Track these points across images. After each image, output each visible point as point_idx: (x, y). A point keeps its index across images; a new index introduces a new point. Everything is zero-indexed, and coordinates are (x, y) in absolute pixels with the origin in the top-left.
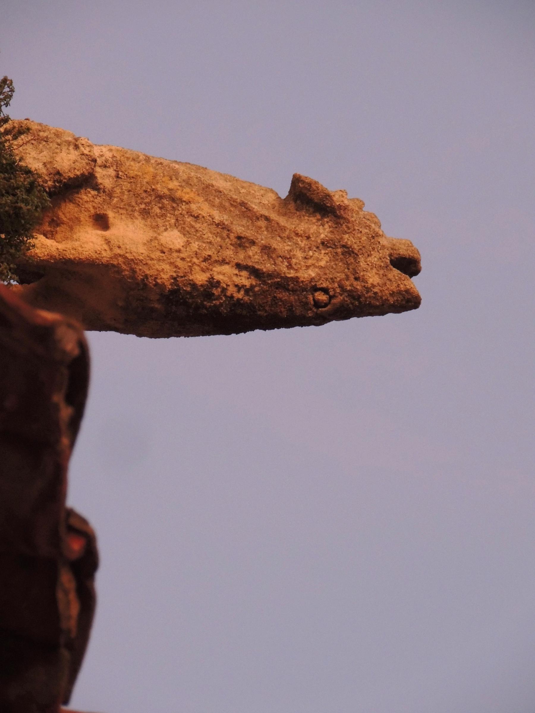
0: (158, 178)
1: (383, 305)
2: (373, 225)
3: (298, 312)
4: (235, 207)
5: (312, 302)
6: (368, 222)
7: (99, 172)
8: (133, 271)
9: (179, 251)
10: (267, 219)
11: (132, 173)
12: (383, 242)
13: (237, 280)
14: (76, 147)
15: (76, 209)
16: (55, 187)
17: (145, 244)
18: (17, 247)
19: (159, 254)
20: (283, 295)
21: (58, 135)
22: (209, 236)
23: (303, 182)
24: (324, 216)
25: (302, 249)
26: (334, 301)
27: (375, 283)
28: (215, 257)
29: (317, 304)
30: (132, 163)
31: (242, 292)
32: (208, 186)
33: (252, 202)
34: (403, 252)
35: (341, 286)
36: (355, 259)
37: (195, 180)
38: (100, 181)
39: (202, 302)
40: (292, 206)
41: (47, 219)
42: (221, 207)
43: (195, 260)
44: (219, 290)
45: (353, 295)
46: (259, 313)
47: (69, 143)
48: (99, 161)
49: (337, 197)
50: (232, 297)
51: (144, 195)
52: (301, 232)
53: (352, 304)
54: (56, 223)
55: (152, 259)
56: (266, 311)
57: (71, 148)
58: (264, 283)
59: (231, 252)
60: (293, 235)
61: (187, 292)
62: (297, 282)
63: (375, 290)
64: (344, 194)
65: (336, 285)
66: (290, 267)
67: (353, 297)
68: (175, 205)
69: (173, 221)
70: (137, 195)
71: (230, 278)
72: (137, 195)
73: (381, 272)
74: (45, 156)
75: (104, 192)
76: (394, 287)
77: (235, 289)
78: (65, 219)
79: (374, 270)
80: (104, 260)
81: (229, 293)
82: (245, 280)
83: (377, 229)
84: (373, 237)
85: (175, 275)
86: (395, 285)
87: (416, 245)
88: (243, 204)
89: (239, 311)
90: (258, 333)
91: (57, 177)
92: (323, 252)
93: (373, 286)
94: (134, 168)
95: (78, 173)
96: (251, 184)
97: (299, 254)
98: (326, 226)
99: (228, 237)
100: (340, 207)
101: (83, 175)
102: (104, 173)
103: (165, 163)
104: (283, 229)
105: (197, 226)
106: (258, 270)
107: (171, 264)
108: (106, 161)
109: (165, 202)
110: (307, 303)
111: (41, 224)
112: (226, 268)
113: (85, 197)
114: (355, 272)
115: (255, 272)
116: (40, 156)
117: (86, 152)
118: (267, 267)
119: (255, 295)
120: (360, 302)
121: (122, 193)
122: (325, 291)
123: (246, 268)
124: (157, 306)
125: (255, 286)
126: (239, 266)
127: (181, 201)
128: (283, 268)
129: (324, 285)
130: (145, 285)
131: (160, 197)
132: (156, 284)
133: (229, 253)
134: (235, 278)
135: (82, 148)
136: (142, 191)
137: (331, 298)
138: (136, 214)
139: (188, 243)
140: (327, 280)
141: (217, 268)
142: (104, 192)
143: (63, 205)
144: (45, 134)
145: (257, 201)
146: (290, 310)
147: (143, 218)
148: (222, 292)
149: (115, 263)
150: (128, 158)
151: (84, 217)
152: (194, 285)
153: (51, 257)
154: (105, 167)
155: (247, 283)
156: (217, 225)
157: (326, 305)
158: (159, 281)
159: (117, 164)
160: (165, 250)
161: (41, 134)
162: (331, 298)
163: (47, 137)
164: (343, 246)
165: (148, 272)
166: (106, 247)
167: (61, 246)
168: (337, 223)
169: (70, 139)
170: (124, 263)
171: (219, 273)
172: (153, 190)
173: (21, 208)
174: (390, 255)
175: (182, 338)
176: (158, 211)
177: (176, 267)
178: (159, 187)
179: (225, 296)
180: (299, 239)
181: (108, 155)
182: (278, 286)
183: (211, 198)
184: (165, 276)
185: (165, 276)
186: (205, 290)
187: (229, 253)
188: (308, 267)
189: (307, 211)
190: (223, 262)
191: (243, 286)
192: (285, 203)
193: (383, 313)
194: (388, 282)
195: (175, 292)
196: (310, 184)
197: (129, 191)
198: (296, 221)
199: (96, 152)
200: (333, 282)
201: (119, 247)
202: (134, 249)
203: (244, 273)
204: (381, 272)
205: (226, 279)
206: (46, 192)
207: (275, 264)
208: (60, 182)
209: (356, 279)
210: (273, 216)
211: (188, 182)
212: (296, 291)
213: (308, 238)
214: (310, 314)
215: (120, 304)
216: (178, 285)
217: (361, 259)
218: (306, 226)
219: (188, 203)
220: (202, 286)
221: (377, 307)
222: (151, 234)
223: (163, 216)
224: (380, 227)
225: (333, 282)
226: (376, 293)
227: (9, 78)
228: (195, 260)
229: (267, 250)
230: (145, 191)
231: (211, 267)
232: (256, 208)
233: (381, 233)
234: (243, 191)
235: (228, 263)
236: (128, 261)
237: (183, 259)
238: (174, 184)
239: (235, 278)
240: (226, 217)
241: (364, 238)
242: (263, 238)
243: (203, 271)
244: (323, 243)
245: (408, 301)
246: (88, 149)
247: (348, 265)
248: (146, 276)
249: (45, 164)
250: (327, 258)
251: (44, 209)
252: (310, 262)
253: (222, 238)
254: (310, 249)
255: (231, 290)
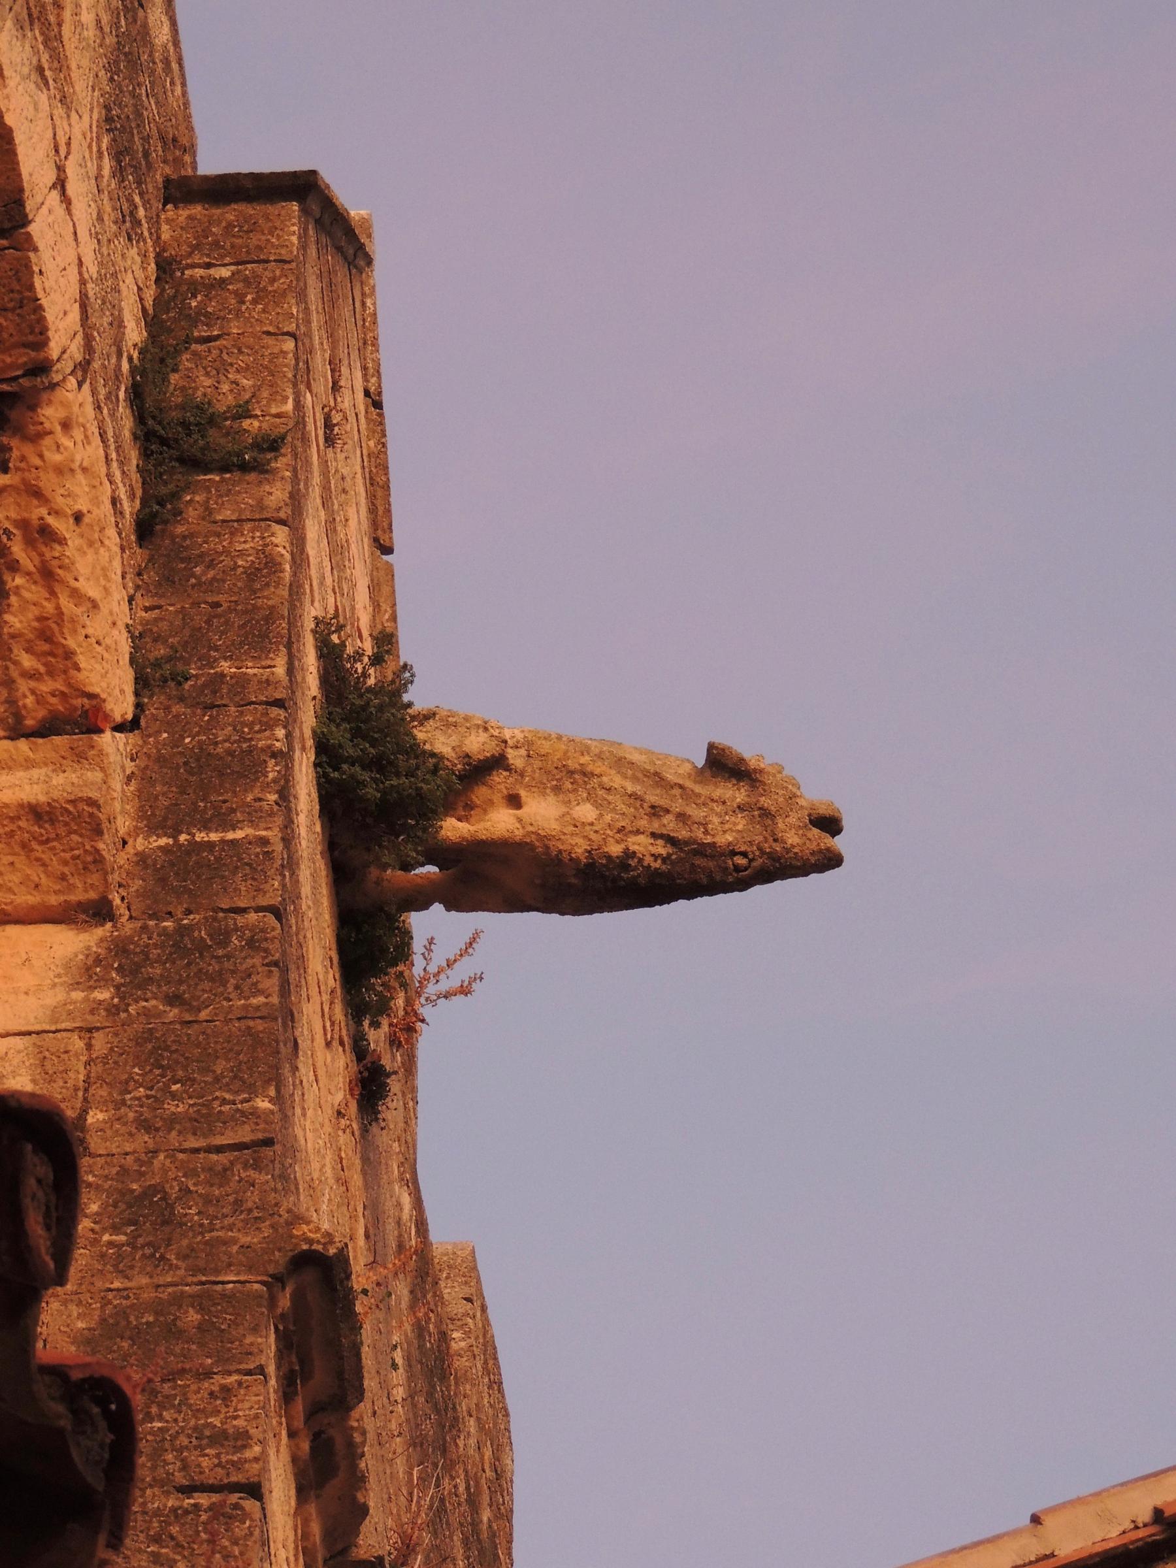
0: (570, 754)
1: (804, 865)
2: (790, 787)
3: (718, 878)
4: (648, 777)
5: (732, 866)
6: (785, 784)
7: (511, 754)
8: (547, 848)
9: (592, 824)
10: (681, 787)
11: (543, 752)
12: (802, 802)
13: (653, 850)
14: (486, 729)
15: (489, 792)
16: (465, 770)
17: (557, 820)
18: (425, 830)
19: (572, 828)
20: (699, 861)
21: (467, 719)
22: (622, 807)
23: (717, 748)
24: (739, 780)
25: (719, 815)
26: (754, 864)
27: (795, 844)
28: (629, 828)
29: (737, 869)
30: (544, 742)
31: (659, 861)
32: (620, 759)
33: (667, 772)
34: (823, 811)
35: (759, 849)
36: (772, 820)
37: (608, 754)
38: (511, 761)
39: (619, 874)
40: (708, 773)
41: (462, 804)
42: (635, 779)
43: (608, 832)
44: (636, 860)
45: (773, 857)
46: (678, 881)
47: (478, 726)
48: (510, 742)
49: (753, 761)
50: (649, 866)
51: (555, 771)
52: (716, 798)
53: (772, 865)
54: (470, 807)
55: (565, 834)
56: (685, 879)
57: (480, 731)
58: (681, 850)
59: (646, 822)
60: (708, 801)
61: (604, 865)
62: (715, 847)
63: (796, 850)
64: (761, 759)
65: (755, 848)
66: (706, 832)
67: (774, 860)
68: (586, 779)
69: (585, 795)
70: (548, 772)
71: (645, 847)
72: (548, 772)
73: (801, 832)
74: (454, 740)
75: (516, 772)
76: (814, 846)
77: (652, 859)
78: (478, 802)
79: (793, 831)
80: (517, 839)
81: (645, 864)
82: (661, 849)
83: (794, 790)
84: (790, 798)
85: (589, 848)
86: (815, 843)
87: (837, 805)
88: (656, 774)
89: (657, 881)
90: (682, 903)
91: (467, 759)
92: (740, 816)
93: (793, 846)
94: (546, 746)
95: (488, 755)
96: (667, 756)
97: (716, 820)
98: (742, 790)
99: (641, 806)
100: (755, 770)
101: (493, 756)
102: (516, 753)
103: (577, 740)
104: (699, 795)
105: (610, 798)
106: (673, 837)
107: (585, 837)
108: (518, 742)
109: (576, 776)
110: (727, 868)
111: (455, 809)
112: (641, 838)
113: (496, 779)
114: (773, 834)
115: (671, 840)
116: (448, 741)
117: (496, 733)
118: (683, 834)
119: (673, 863)
120: (780, 863)
121: (533, 771)
122: (744, 854)
123: (661, 836)
124: (573, 881)
125: (672, 855)
126: (654, 835)
127: (593, 774)
128: (699, 834)
129: (743, 849)
130: (560, 861)
131: (571, 773)
132: (571, 859)
133: (643, 823)
134: (650, 848)
135: (492, 731)
136: (553, 768)
137: (751, 861)
138: (548, 791)
139: (601, 815)
140: (745, 843)
141: (632, 839)
142: (516, 772)
143: (476, 788)
144: (454, 720)
145: (673, 771)
146: (710, 876)
147: (555, 795)
148: (639, 862)
149: (528, 841)
150: (540, 738)
151: (497, 798)
152: (609, 857)
153: (463, 838)
154: (517, 747)
155: (663, 852)
156: (630, 796)
157: (746, 870)
158: (573, 855)
159: (528, 744)
160: (578, 824)
161: (450, 719)
162: (751, 861)
163: (456, 722)
164: (760, 809)
165: (561, 847)
166: (518, 825)
167: (472, 828)
168: (753, 787)
169: (480, 722)
170: (537, 840)
171: (634, 844)
172: (564, 766)
173: (422, 788)
174: (810, 815)
175: (606, 914)
176: (570, 786)
177: (590, 840)
178: (570, 762)
179: (642, 866)
180: (715, 805)
181: (520, 736)
182: (696, 853)
183: (624, 770)
184: (580, 851)
185: (580, 851)
186: (621, 862)
187: (643, 823)
188: (725, 832)
189: (723, 777)
190: (638, 832)
191: (660, 855)
192: (700, 772)
193: (806, 874)
194: (808, 842)
195: (591, 866)
196: (723, 750)
197: (541, 769)
198: (711, 787)
199: (507, 734)
200: (752, 845)
201: (531, 825)
202: (546, 826)
203: (660, 842)
204: (801, 832)
205: (641, 849)
206: (456, 775)
207: (691, 831)
208: (469, 764)
209: (775, 840)
210: (689, 784)
211: (600, 756)
212: (714, 856)
213: (724, 803)
214: (730, 879)
215: (538, 881)
216: (593, 859)
217: (779, 820)
218: (722, 791)
219: (599, 776)
220: (617, 857)
221: (798, 868)
222: (564, 809)
223: (575, 790)
224: (799, 788)
225: (752, 845)
226: (796, 854)
227: (409, 663)
228: (608, 832)
229: (682, 817)
230: (556, 768)
231: (625, 838)
232: (670, 777)
233: (799, 794)
234: (658, 762)
235: (643, 833)
236: (541, 838)
237: (596, 832)
238: (585, 759)
239: (650, 848)
240: (639, 788)
241: (781, 799)
242: (678, 806)
243: (618, 842)
244: (739, 807)
245: (830, 859)
246: (497, 731)
247: (766, 827)
248: (560, 851)
249: (453, 748)
250: (744, 822)
251: (458, 793)
252: (727, 826)
253: (636, 808)
254: (726, 813)
255: (648, 860)
